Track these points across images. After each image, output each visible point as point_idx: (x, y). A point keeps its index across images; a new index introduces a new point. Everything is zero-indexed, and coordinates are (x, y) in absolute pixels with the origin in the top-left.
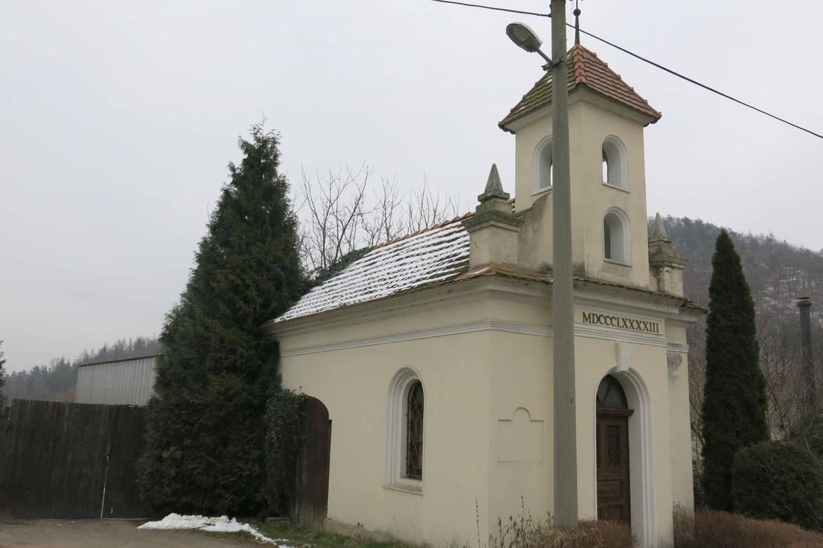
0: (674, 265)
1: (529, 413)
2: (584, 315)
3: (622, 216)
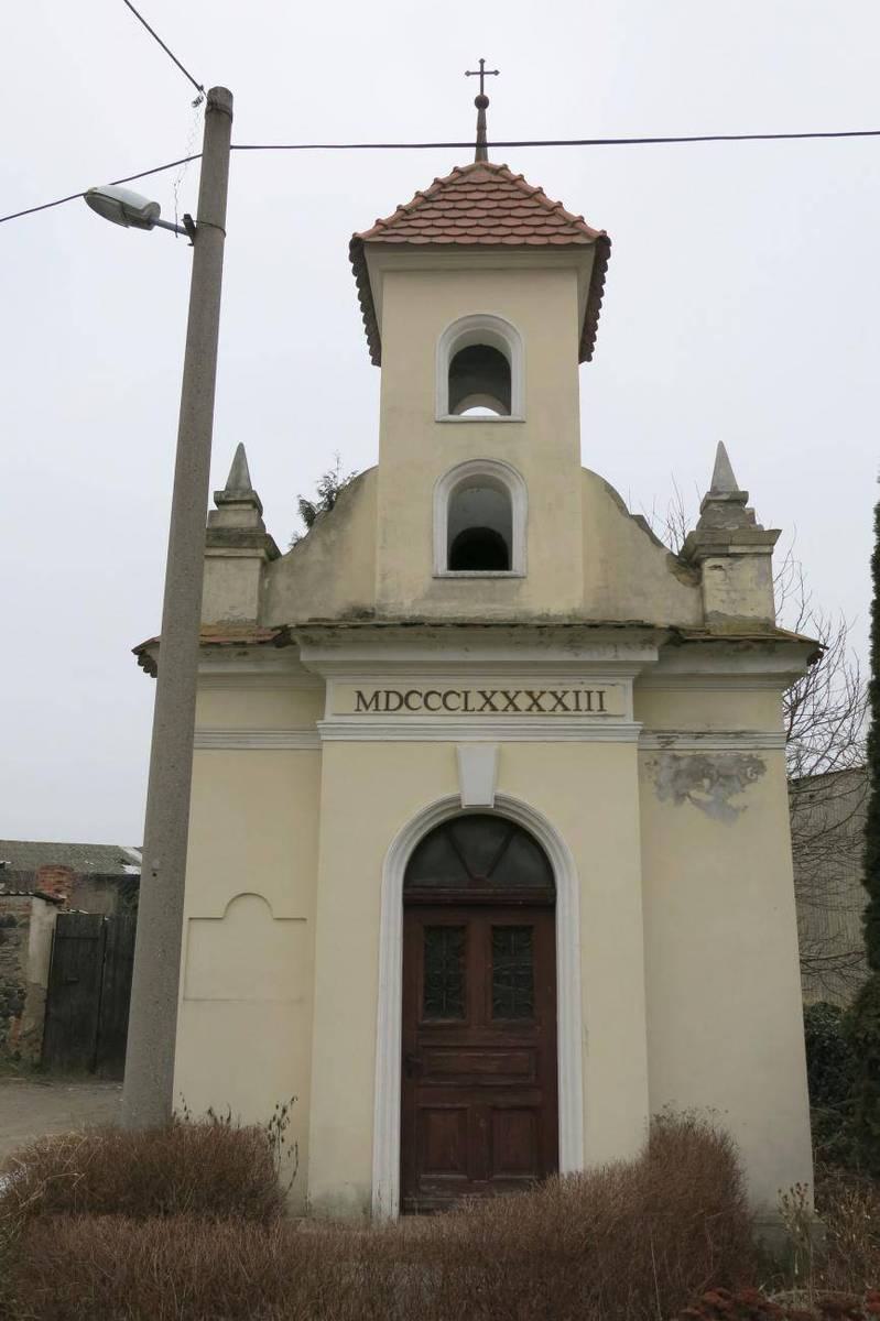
0: (732, 550)
1: (265, 900)
2: (360, 694)
3: (500, 472)
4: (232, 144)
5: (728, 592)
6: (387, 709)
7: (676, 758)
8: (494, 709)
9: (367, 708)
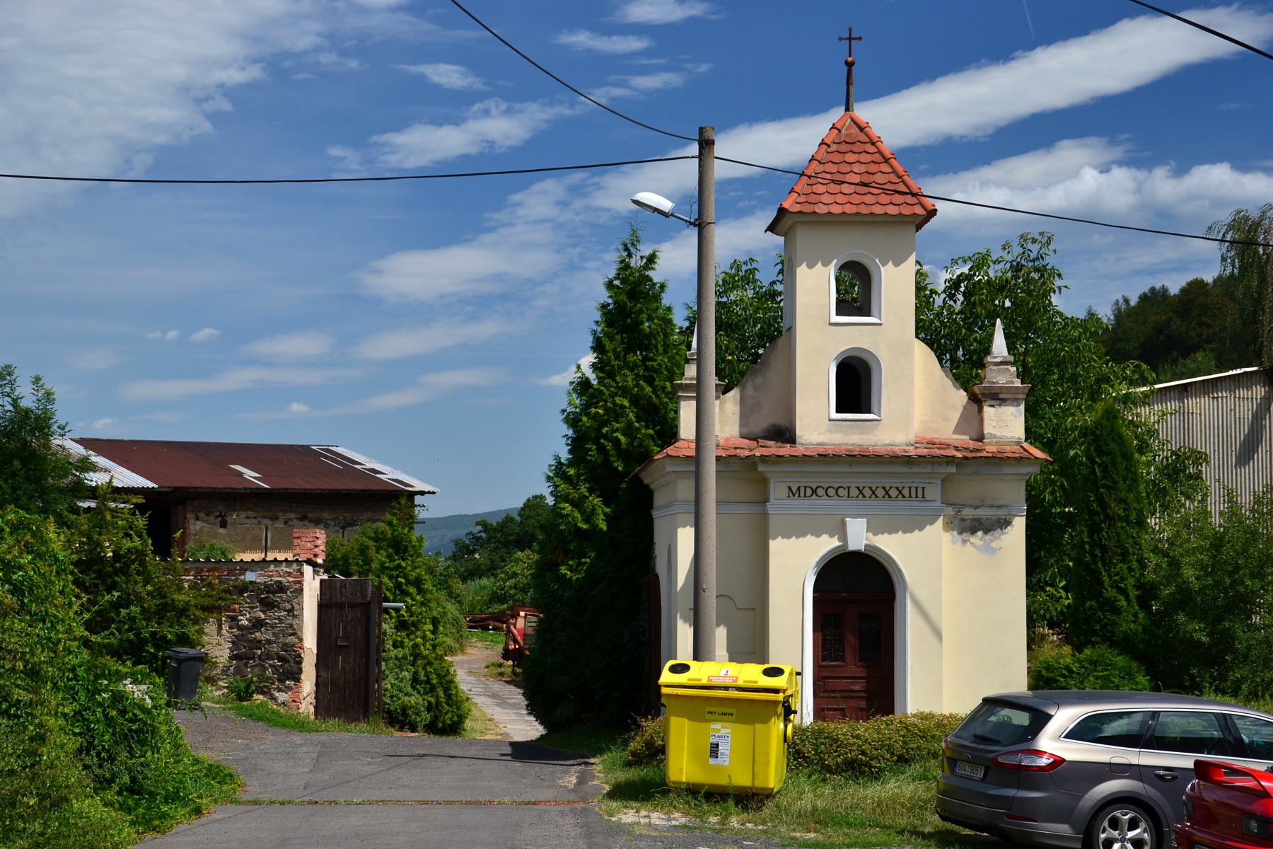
0: (1001, 396)
2: (790, 488)
4: (715, 155)
5: (997, 422)
6: (805, 496)
7: (963, 520)
8: (864, 496)
9: (794, 495)
